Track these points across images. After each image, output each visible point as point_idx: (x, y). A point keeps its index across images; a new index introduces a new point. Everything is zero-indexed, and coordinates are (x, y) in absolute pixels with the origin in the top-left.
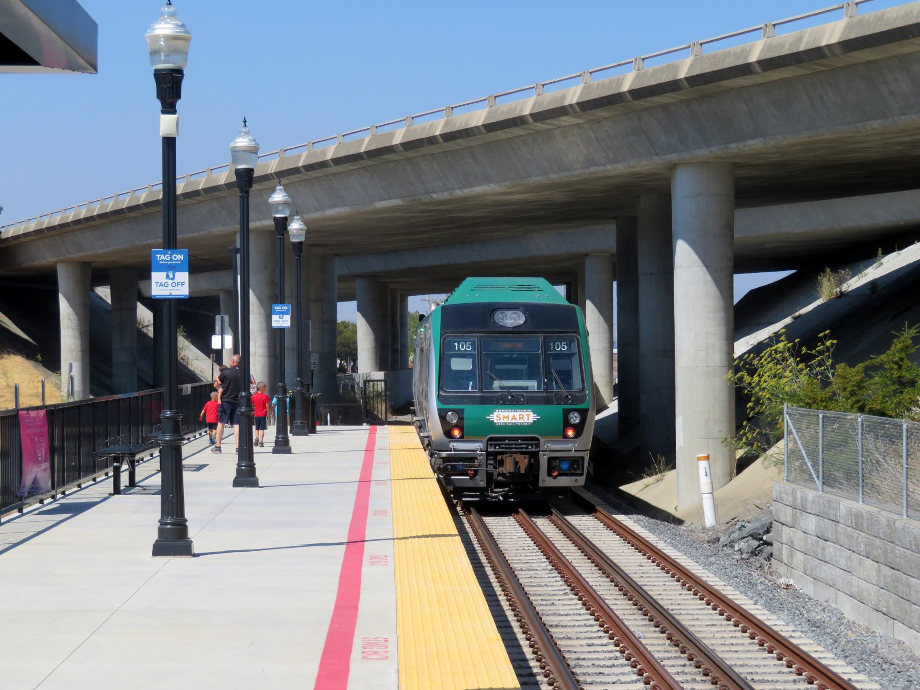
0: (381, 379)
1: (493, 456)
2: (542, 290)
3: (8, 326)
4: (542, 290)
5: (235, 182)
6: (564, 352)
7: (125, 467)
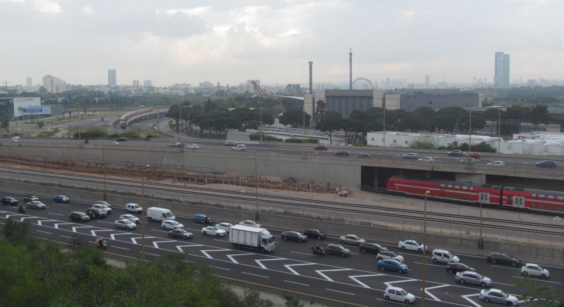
1: (475, 269)
2: (311, 64)
4: (311, 64)
5: (504, 196)
7: (395, 184)
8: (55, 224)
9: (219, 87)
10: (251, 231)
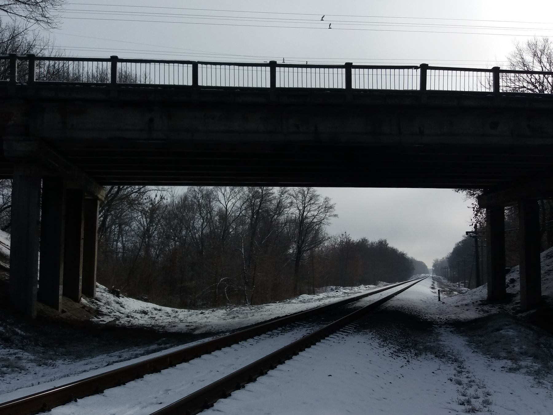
0: (478, 89)
3: (266, 62)
6: (95, 283)
8: (352, 69)
9: (161, 372)
10: (69, 383)
